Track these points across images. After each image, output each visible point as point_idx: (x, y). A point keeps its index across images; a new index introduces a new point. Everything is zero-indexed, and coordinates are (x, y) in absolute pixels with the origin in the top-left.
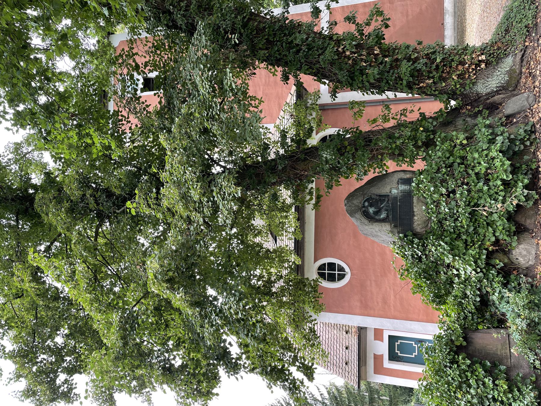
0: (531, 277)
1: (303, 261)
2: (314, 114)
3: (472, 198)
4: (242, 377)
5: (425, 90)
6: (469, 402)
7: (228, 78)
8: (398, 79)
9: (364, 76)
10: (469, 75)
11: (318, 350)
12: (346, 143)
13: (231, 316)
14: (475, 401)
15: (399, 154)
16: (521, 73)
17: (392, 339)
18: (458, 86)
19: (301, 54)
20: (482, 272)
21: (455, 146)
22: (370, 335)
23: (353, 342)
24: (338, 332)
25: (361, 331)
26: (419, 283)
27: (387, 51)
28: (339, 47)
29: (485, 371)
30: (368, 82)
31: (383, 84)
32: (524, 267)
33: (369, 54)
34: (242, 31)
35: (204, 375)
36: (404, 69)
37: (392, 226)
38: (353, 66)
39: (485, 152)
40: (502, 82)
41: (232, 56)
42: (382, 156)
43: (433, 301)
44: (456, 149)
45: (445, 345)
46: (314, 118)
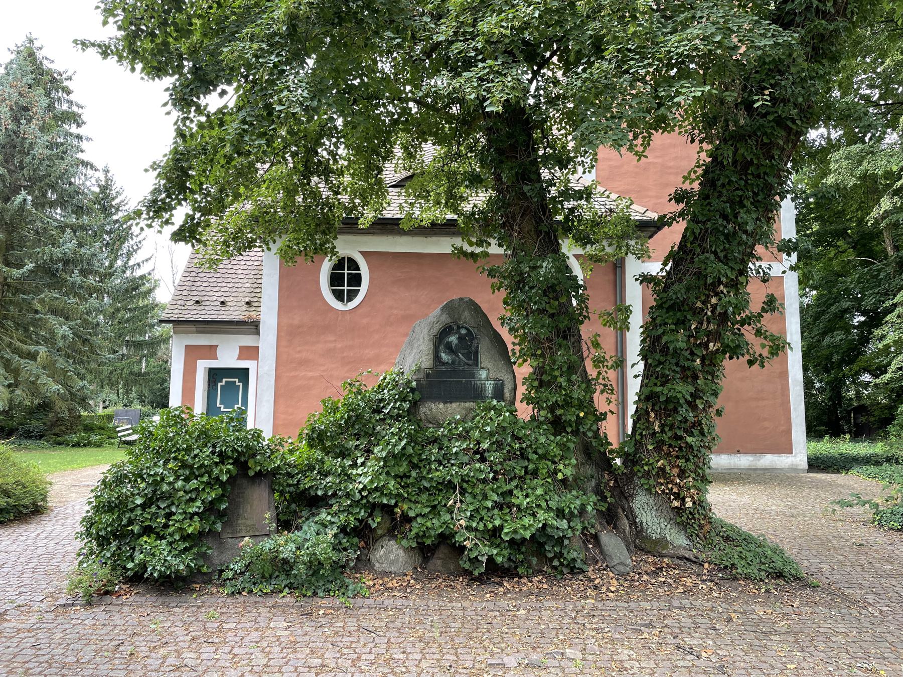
0: (356, 565)
1: (363, 232)
2: (609, 250)
3: (474, 486)
4: (168, 113)
5: (643, 420)
6: (163, 479)
7: (693, 89)
8: (664, 379)
9: (673, 327)
10: (662, 484)
11: (219, 253)
12: (563, 300)
13: (275, 91)
14: (165, 487)
15: (542, 381)
16: (662, 556)
17: (243, 374)
18: (646, 468)
19: (720, 221)
20: (362, 499)
21: (554, 463)
22: (247, 340)
23: (235, 313)
24: (248, 290)
25: (253, 327)
26: (341, 409)
27: (711, 363)
28: (726, 286)
29: (211, 502)
30: (664, 333)
31: (658, 356)
32: (371, 556)
33: (709, 334)
34: (771, 118)
35: (166, 44)
36: (680, 388)
37: (428, 371)
38: (691, 309)
39: (544, 504)
40: (649, 530)
41: (731, 97)
42: (540, 356)
43: (313, 430)
44: (550, 463)
45: (247, 446)
46: (604, 249)
